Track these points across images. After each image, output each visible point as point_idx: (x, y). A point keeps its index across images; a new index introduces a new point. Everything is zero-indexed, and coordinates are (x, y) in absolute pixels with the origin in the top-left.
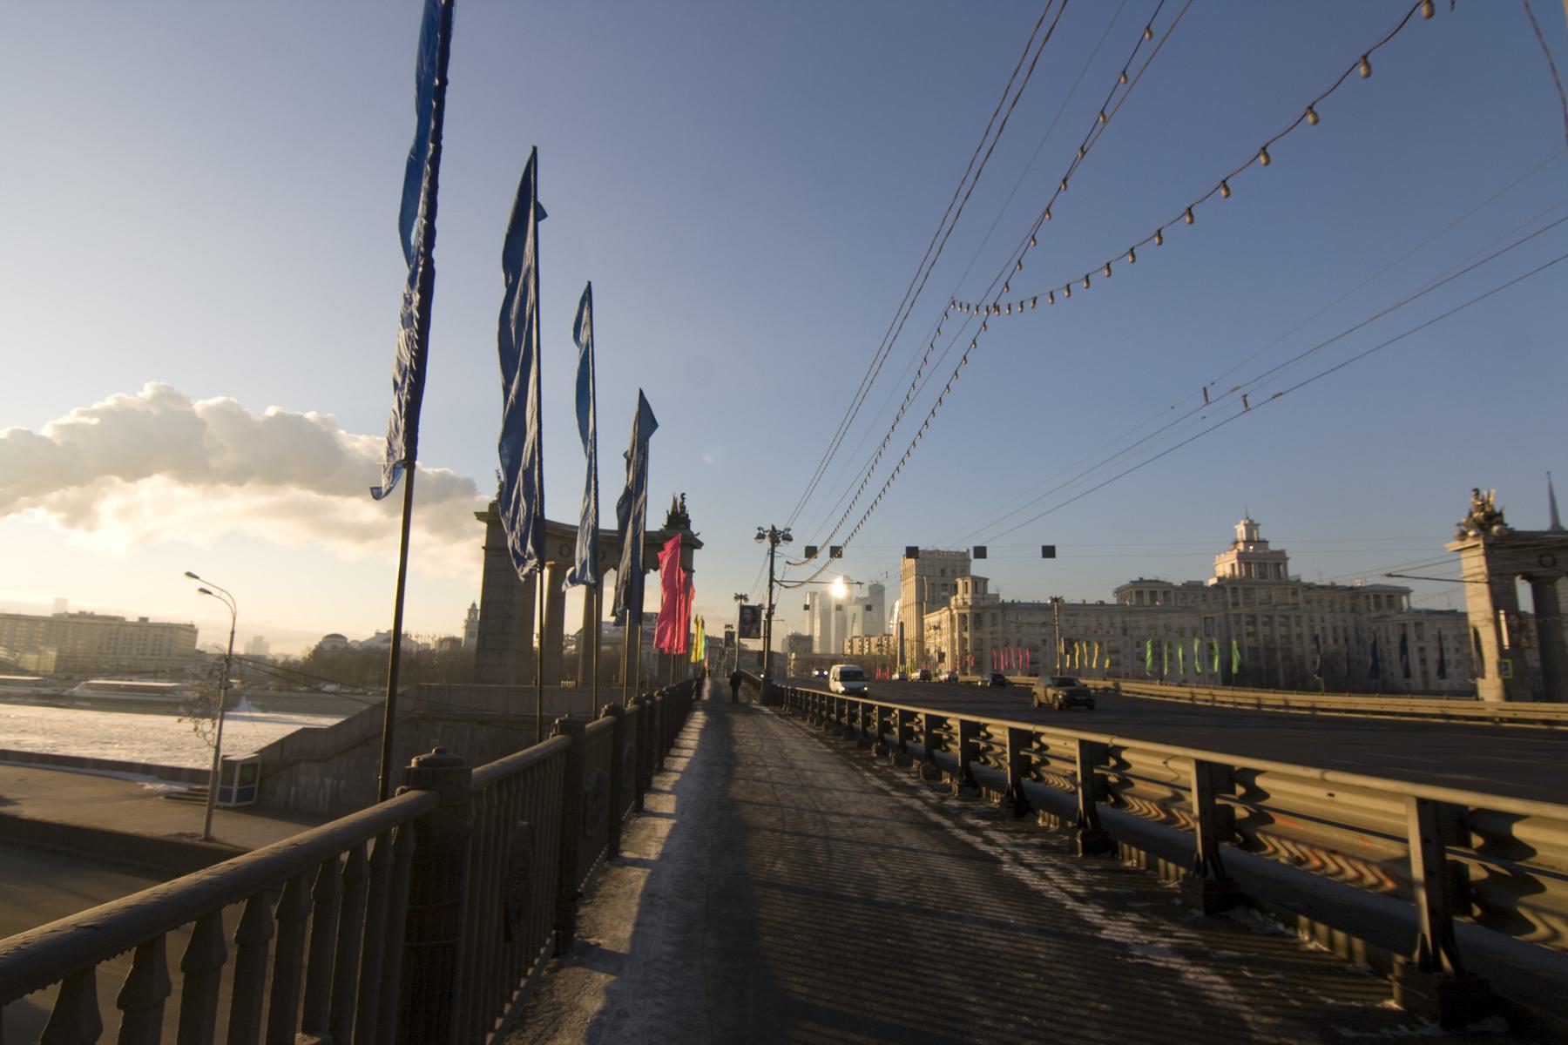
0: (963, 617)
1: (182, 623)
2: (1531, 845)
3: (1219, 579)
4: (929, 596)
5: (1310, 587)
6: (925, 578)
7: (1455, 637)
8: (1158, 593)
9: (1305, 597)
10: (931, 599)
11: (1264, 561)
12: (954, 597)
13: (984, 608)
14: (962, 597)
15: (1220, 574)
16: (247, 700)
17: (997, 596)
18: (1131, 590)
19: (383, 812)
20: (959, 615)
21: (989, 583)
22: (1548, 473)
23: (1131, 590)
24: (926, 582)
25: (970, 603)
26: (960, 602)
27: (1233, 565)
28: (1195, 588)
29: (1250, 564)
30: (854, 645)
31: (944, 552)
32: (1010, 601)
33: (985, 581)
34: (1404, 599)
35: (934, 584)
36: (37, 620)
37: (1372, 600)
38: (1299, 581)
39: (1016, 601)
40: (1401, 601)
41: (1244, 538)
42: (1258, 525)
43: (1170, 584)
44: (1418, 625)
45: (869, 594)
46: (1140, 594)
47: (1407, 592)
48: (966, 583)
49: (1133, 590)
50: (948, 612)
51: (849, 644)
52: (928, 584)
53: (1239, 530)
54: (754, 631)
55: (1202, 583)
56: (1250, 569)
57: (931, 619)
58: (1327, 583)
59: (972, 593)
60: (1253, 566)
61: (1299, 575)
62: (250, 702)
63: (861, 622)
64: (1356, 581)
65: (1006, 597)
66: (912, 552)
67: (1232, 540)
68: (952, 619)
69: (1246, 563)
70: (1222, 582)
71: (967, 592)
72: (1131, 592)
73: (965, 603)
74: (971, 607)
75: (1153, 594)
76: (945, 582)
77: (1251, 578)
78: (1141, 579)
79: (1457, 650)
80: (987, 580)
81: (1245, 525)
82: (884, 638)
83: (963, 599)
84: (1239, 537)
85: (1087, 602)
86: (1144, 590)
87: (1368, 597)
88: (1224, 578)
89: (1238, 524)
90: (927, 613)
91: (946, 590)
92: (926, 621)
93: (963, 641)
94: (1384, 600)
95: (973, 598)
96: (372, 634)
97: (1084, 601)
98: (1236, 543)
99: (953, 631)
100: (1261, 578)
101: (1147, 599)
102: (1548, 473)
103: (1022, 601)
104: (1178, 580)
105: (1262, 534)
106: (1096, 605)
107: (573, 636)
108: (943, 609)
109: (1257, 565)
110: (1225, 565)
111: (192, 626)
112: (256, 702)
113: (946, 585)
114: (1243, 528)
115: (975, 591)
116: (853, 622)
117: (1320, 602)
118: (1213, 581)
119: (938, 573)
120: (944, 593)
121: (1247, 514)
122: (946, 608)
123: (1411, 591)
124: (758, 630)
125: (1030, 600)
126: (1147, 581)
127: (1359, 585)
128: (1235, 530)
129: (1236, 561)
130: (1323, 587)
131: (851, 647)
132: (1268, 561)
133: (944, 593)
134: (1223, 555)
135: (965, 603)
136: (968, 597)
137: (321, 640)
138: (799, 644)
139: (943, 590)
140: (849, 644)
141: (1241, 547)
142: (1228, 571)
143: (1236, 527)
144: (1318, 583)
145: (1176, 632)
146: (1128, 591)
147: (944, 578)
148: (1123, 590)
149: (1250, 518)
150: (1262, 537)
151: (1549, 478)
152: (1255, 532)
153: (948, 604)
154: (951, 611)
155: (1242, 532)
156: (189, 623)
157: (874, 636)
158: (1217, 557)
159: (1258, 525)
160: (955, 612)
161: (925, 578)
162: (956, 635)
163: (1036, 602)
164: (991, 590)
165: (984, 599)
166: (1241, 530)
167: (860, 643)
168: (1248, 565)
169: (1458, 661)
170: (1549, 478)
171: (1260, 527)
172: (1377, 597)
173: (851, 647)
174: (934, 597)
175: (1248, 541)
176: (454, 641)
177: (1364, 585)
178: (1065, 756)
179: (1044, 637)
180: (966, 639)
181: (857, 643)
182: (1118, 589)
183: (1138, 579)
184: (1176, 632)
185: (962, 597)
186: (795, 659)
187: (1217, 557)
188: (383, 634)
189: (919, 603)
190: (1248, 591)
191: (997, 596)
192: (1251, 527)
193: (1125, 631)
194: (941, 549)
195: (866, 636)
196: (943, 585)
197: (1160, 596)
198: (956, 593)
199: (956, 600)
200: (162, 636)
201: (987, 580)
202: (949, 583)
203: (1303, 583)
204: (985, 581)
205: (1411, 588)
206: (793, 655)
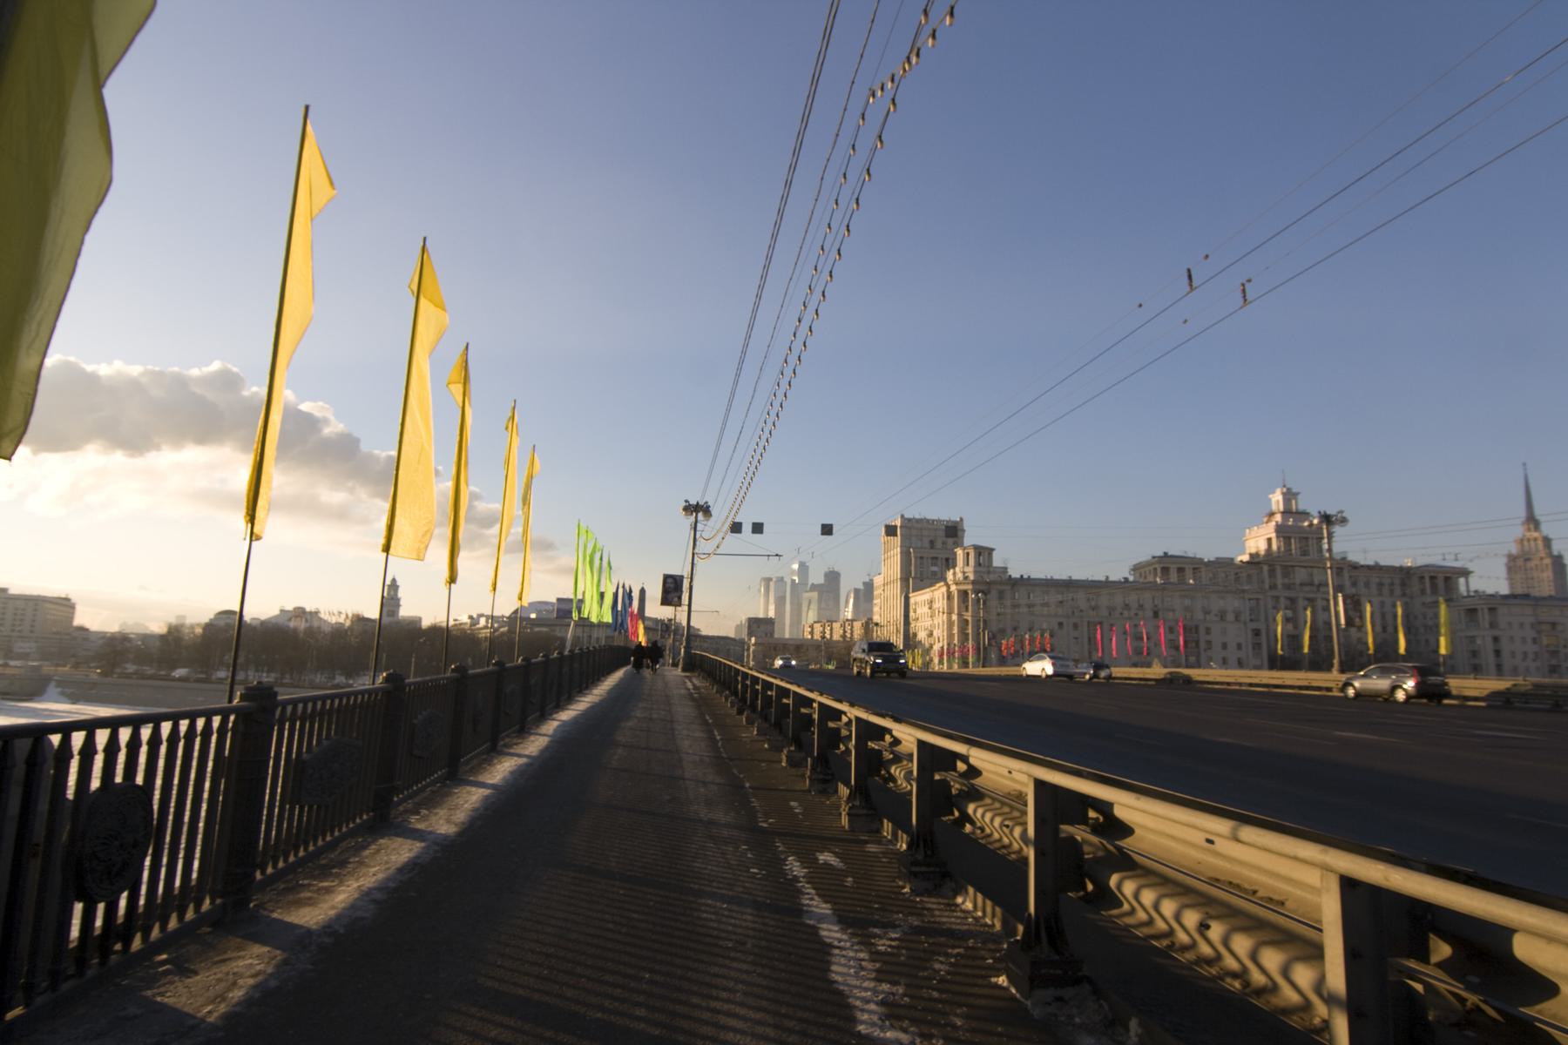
0: (964, 595)
1: (56, 595)
2: (1132, 825)
3: (1251, 555)
4: (915, 570)
5: (1355, 567)
6: (911, 550)
7: (1532, 626)
8: (1171, 570)
9: (1350, 577)
10: (919, 576)
11: (1305, 535)
12: (952, 571)
13: (989, 584)
14: (962, 570)
15: (1253, 551)
16: (57, 686)
17: (1005, 569)
18: (1157, 566)
19: (601, 701)
20: (959, 591)
21: (994, 553)
22: (1524, 464)
23: (1157, 566)
24: (912, 555)
25: (972, 577)
26: (960, 576)
27: (1269, 540)
28: (1225, 564)
29: (1290, 538)
30: (815, 630)
31: (933, 521)
32: (1018, 576)
33: (990, 551)
34: (1462, 581)
35: (922, 558)
36: (37, 600)
37: (1427, 581)
38: (1344, 559)
39: (1025, 576)
40: (1457, 584)
41: (1281, 508)
42: (1298, 494)
43: (1201, 560)
44: (1492, 610)
45: (825, 581)
46: (1165, 570)
47: (1465, 573)
48: (968, 554)
49: (1158, 567)
50: (944, 589)
51: (809, 629)
52: (916, 558)
53: (1274, 500)
54: (676, 599)
55: (1232, 559)
56: (1290, 544)
57: (919, 598)
58: (1371, 563)
59: (975, 566)
60: (1293, 541)
61: (1345, 552)
62: (59, 690)
63: (816, 608)
64: (1406, 561)
65: (1015, 573)
66: (891, 531)
67: (1267, 511)
68: (950, 596)
69: (1284, 538)
70: (1255, 562)
71: (968, 565)
72: (1155, 569)
73: (966, 578)
74: (973, 582)
75: (1181, 570)
76: (935, 555)
77: (1291, 554)
78: (1166, 554)
79: (1535, 641)
80: (992, 550)
81: (1284, 494)
82: (827, 625)
83: (964, 573)
84: (1274, 508)
85: (1111, 579)
86: (1187, 566)
87: (1422, 578)
88: (1257, 554)
89: (1274, 492)
90: (913, 592)
91: (935, 565)
92: (912, 601)
93: (964, 623)
94: (1440, 583)
95: (975, 572)
96: (277, 612)
97: (1107, 577)
98: (1272, 514)
99: (950, 613)
100: (1301, 555)
101: (1174, 577)
102: (1524, 464)
103: (1032, 577)
104: (1208, 554)
105: (1302, 504)
106: (1120, 582)
107: (507, 618)
108: (938, 585)
109: (1297, 540)
110: (1258, 540)
111: (67, 600)
112: (66, 690)
113: (936, 558)
114: (1280, 498)
115: (978, 564)
116: (808, 609)
117: (1367, 585)
118: (1246, 558)
119: (927, 545)
120: (934, 569)
121: (1284, 480)
122: (942, 584)
123: (1472, 572)
124: (680, 598)
125: (1042, 576)
126: (1172, 556)
127: (1409, 564)
128: (1270, 500)
129: (1273, 535)
130: (1368, 567)
131: (812, 633)
132: (1310, 536)
133: (934, 569)
134: (1255, 528)
135: (966, 578)
136: (970, 570)
137: (212, 617)
138: (759, 627)
139: (932, 565)
140: (809, 629)
141: (1278, 518)
142: (1262, 546)
143: (1271, 496)
144: (1362, 563)
145: (1216, 615)
146: (1151, 568)
147: (932, 551)
148: (1144, 567)
149: (1288, 486)
150: (1301, 507)
151: (1525, 469)
152: (1294, 502)
153: (944, 579)
154: (948, 586)
155: (1278, 501)
156: (63, 596)
157: (836, 621)
158: (1248, 531)
159: (1298, 494)
160: (953, 588)
161: (911, 550)
162: (955, 617)
163: (1049, 577)
164: (997, 561)
165: (989, 572)
166: (1277, 500)
167: (821, 629)
168: (1287, 540)
169: (1536, 654)
170: (1525, 469)
171: (1299, 497)
172: (1432, 578)
173: (812, 633)
174: (921, 574)
175: (1287, 512)
176: (359, 620)
177: (1414, 566)
178: (1259, 845)
179: (1061, 620)
180: (967, 621)
181: (818, 628)
182: (1134, 566)
183: (1162, 554)
184: (1216, 615)
185: (962, 570)
186: (755, 645)
187: (1248, 531)
188: (289, 611)
189: (905, 579)
190: (1288, 570)
191: (1005, 569)
192: (1289, 496)
193: (1156, 614)
194: (929, 517)
195: (828, 621)
196: (933, 558)
197: (1189, 573)
198: (954, 566)
199: (954, 574)
200: (24, 610)
201: (992, 550)
202: (940, 556)
203: (1350, 561)
204: (990, 551)
205: (1471, 569)
206: (753, 640)
